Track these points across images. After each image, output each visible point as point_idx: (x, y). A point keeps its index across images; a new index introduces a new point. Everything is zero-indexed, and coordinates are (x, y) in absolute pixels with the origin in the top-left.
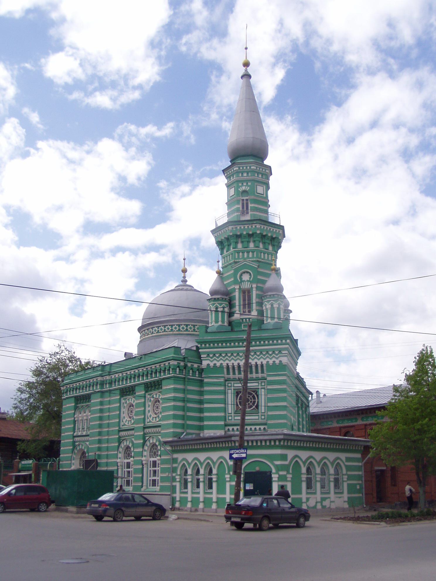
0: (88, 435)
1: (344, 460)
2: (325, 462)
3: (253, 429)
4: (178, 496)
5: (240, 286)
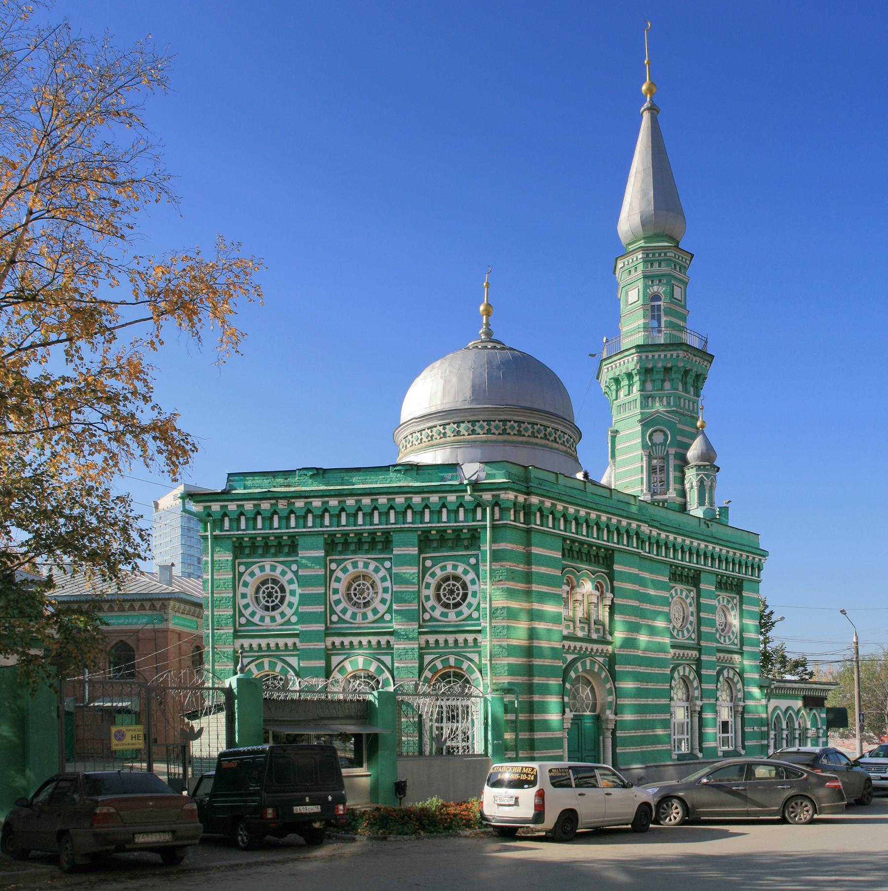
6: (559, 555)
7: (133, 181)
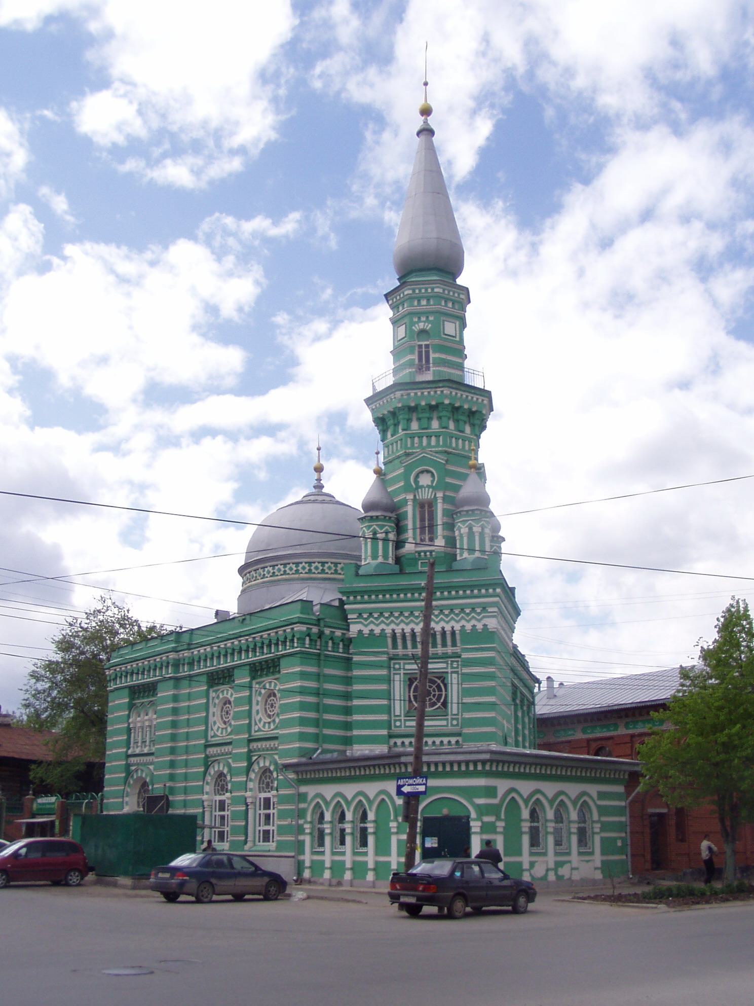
0: (152, 754)
1: (595, 796)
2: (562, 800)
4: (307, 858)
5: (415, 496)
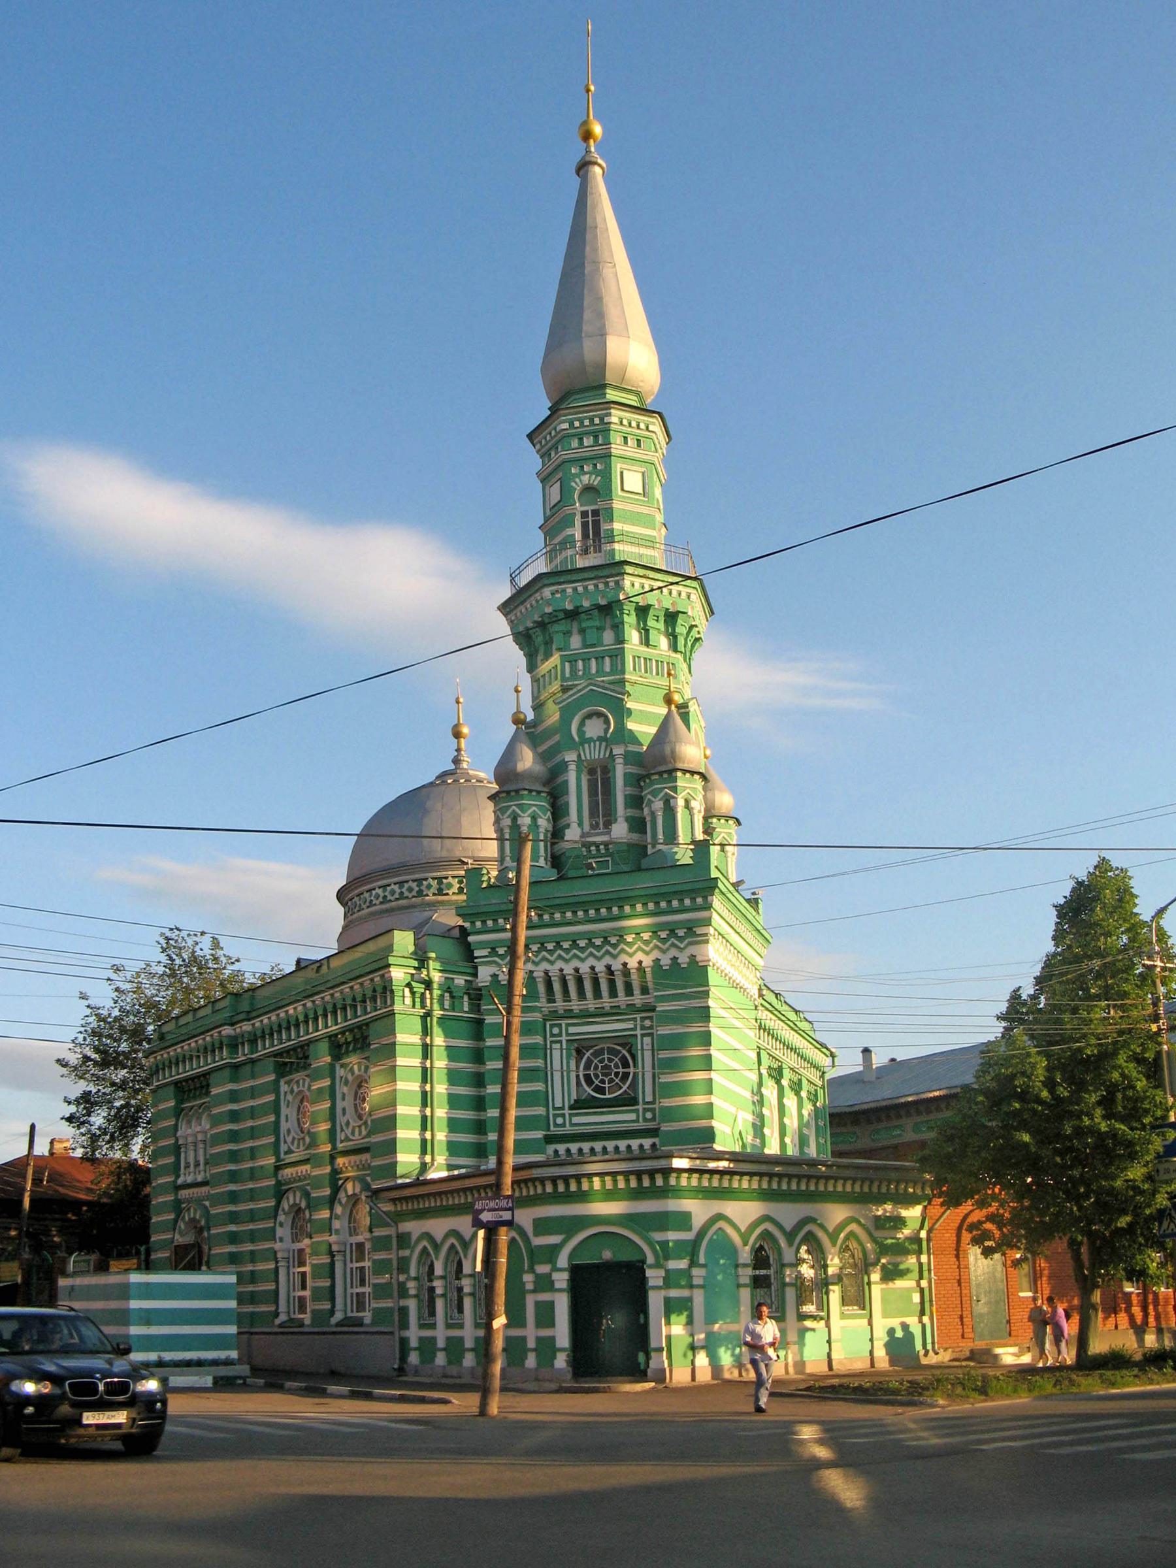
0: (205, 1183)
3: (623, 1148)
4: (414, 1334)
5: (579, 756)
6: (233, 1304)
7: (1009, 1322)
